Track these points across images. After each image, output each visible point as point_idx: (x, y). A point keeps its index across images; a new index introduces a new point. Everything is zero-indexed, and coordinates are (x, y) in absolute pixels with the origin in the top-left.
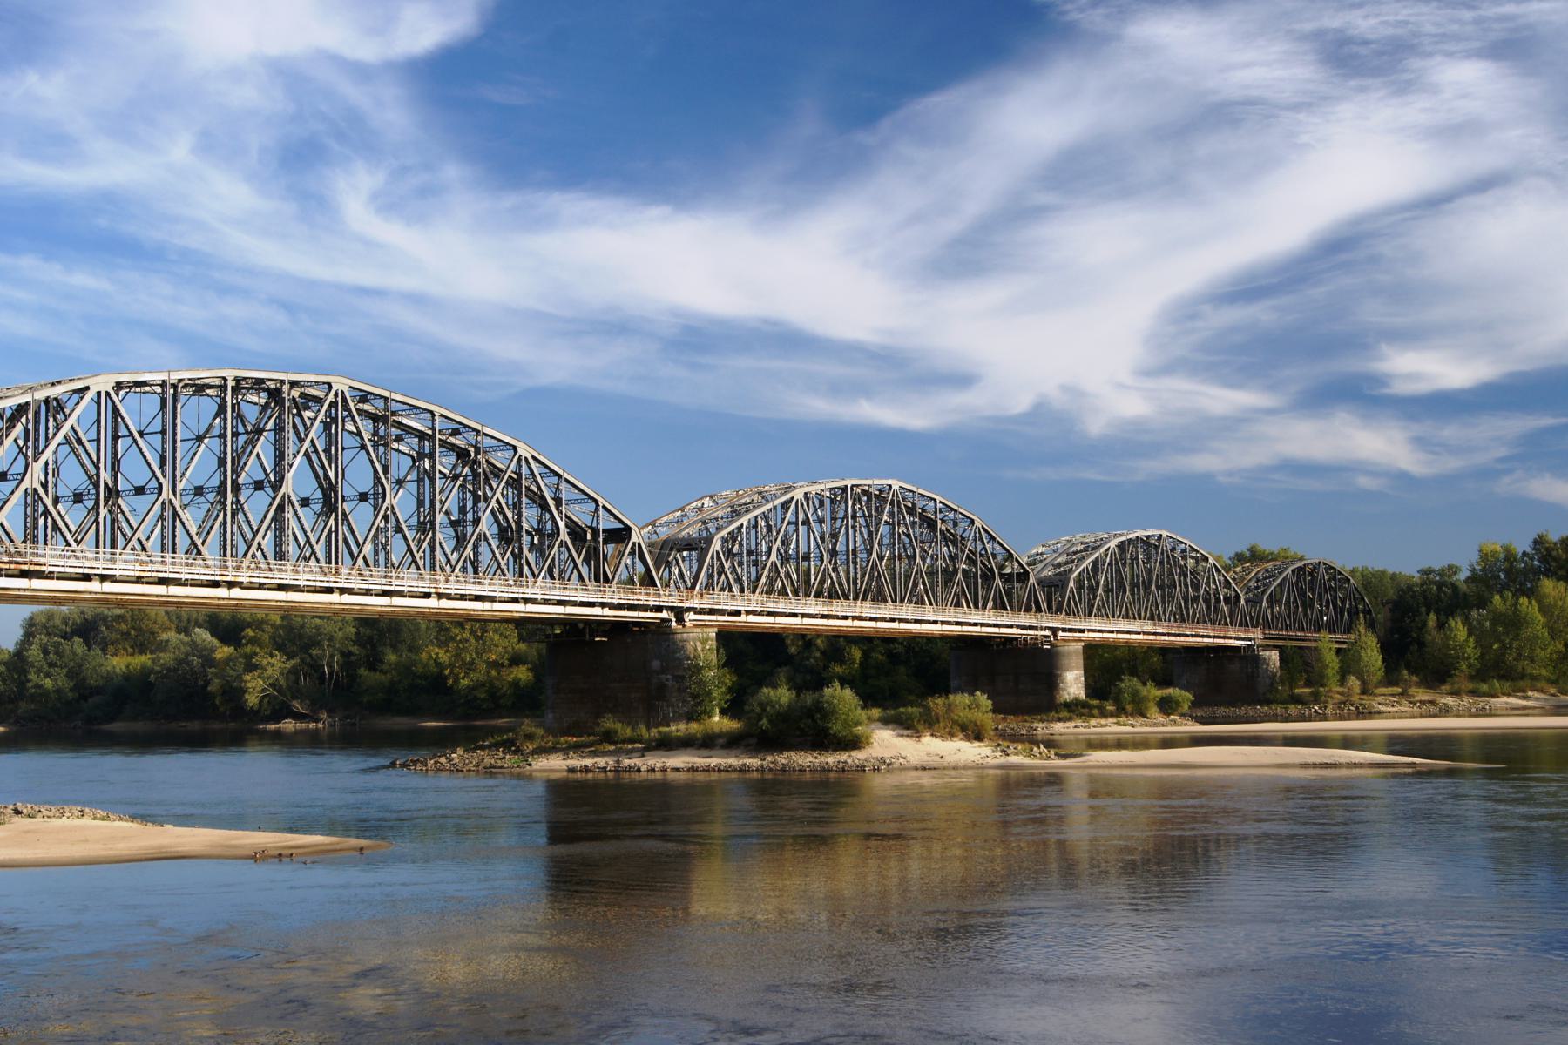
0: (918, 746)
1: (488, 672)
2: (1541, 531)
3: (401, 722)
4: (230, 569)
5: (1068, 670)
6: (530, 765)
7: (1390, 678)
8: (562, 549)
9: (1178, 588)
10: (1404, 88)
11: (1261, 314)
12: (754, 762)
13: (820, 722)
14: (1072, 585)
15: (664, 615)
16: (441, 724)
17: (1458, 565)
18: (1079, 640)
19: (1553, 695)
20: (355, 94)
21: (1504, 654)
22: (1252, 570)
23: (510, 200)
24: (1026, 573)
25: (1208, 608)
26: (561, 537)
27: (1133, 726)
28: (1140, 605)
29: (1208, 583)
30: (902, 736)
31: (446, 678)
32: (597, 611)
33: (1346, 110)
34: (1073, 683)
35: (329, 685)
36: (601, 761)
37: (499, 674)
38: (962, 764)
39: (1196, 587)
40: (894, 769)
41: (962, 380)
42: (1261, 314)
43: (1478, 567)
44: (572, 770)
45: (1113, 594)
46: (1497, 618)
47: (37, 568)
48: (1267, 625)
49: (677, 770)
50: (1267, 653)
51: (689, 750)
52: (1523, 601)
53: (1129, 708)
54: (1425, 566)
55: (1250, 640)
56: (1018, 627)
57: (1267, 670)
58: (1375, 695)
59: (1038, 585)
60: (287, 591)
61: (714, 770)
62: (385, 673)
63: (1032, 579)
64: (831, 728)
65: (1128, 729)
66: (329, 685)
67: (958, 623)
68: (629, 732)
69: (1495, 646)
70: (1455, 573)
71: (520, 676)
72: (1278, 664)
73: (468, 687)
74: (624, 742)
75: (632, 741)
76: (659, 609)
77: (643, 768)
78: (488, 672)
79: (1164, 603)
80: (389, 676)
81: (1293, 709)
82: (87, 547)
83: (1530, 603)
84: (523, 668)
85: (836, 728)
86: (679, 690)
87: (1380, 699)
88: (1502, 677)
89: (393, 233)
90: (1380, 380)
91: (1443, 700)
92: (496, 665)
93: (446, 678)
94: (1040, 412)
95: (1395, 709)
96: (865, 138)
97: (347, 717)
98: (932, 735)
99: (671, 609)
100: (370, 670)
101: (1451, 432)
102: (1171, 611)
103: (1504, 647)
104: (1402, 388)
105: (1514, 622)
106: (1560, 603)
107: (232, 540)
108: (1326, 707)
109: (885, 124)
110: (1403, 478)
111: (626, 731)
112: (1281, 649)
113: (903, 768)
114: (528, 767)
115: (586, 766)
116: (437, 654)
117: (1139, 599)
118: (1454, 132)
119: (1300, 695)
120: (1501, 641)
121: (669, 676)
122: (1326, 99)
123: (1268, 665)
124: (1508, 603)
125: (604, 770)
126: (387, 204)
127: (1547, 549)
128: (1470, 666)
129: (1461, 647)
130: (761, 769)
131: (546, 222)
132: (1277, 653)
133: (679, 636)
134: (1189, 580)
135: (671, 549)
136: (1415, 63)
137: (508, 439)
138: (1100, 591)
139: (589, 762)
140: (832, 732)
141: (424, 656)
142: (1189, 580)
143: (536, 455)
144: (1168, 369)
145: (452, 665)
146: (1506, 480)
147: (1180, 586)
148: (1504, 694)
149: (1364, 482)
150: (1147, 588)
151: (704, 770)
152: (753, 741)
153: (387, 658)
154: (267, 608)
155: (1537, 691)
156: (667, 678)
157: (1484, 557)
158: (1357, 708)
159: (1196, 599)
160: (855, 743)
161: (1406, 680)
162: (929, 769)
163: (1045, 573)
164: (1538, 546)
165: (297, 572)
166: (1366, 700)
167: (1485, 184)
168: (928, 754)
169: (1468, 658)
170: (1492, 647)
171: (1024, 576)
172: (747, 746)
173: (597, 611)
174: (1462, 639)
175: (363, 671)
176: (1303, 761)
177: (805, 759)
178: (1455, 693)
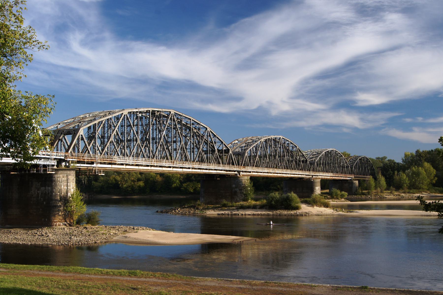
0: (314, 209)
1: (131, 183)
2: (418, 149)
3: (105, 197)
4: (153, 162)
5: (316, 186)
6: (206, 213)
7: (387, 189)
8: (111, 144)
9: (286, 157)
10: (378, 20)
11: (327, 83)
12: (271, 213)
13: (289, 203)
14: (247, 155)
15: (236, 173)
16: (118, 197)
17: (386, 156)
18: (319, 178)
19: (429, 193)
20: (81, 11)
21: (416, 182)
22: (348, 159)
23: (121, 43)
24: (228, 150)
25: (296, 164)
26: (216, 152)
27: (337, 202)
28: (272, 162)
29: (297, 156)
30: (309, 206)
31: (119, 184)
32: (223, 172)
33: (360, 26)
34: (318, 190)
35: (84, 186)
36: (227, 212)
37: (134, 183)
38: (328, 214)
39: (292, 157)
40: (310, 215)
41: (239, 99)
42: (327, 83)
43: (404, 159)
44: (218, 214)
45: (262, 159)
46: (414, 173)
47: (115, 162)
48: (354, 174)
49: (250, 215)
50: (355, 181)
51: (250, 209)
52: (420, 168)
53: (335, 197)
54: (377, 157)
55: (351, 178)
56: (305, 175)
57: (355, 186)
58: (384, 193)
59: (233, 155)
60: (139, 166)
61: (260, 215)
62: (100, 183)
63: (230, 152)
64: (292, 204)
65: (336, 203)
66: (84, 186)
67: (257, 172)
68: (231, 204)
69: (413, 180)
70: (386, 159)
71: (141, 184)
72: (358, 185)
73: (126, 187)
74: (229, 207)
75: (231, 207)
76: (235, 171)
77: (240, 214)
78: (131, 183)
79: (281, 162)
80: (101, 184)
81: (363, 197)
82: (140, 159)
83: (422, 169)
84: (142, 182)
85: (293, 204)
86: (240, 193)
87: (385, 194)
88: (414, 188)
89: (86, 52)
90: (354, 102)
91: (401, 195)
92: (134, 181)
93: (119, 184)
94: (260, 109)
95: (390, 197)
96: (226, 30)
97: (90, 195)
98: (316, 206)
99: (237, 171)
100: (96, 182)
101: (371, 117)
102: (283, 165)
103: (415, 180)
104: (361, 104)
105: (418, 174)
106: (429, 169)
107: (110, 150)
108: (372, 196)
109: (233, 26)
110: (356, 129)
111: (230, 204)
112: (359, 180)
113: (312, 215)
114: (206, 214)
115: (222, 213)
116: (117, 178)
117: (272, 161)
118: (390, 33)
119: (364, 193)
120: (415, 179)
121: (238, 189)
122: (355, 22)
123: (355, 184)
124: (416, 169)
125: (228, 214)
126: (84, 44)
127: (420, 154)
128: (407, 185)
129: (404, 180)
130: (273, 215)
131: (130, 50)
132: (358, 181)
133: (240, 178)
134: (290, 154)
135: (62, 134)
136: (382, 14)
137: (205, 126)
138: (257, 157)
139: (223, 212)
140: (292, 205)
141: (111, 178)
142: (290, 154)
143: (212, 131)
144: (298, 97)
145: (121, 181)
146: (383, 130)
147: (287, 156)
148: (417, 193)
149: (345, 130)
150: (275, 156)
151: (257, 215)
152: (268, 207)
153: (100, 178)
154: (177, 173)
155: (425, 192)
156: (237, 190)
157: (406, 156)
158: (380, 196)
159: (292, 161)
160: (297, 208)
161: (392, 189)
162: (320, 215)
163: (237, 150)
164: (417, 153)
165: (166, 162)
166: (382, 194)
167: (394, 49)
168: (318, 211)
169: (407, 183)
170: (412, 180)
171: (227, 151)
172: (266, 208)
173: (223, 172)
174: (405, 178)
175: (93, 182)
176: (421, 214)
177: (285, 212)
178: (404, 193)
